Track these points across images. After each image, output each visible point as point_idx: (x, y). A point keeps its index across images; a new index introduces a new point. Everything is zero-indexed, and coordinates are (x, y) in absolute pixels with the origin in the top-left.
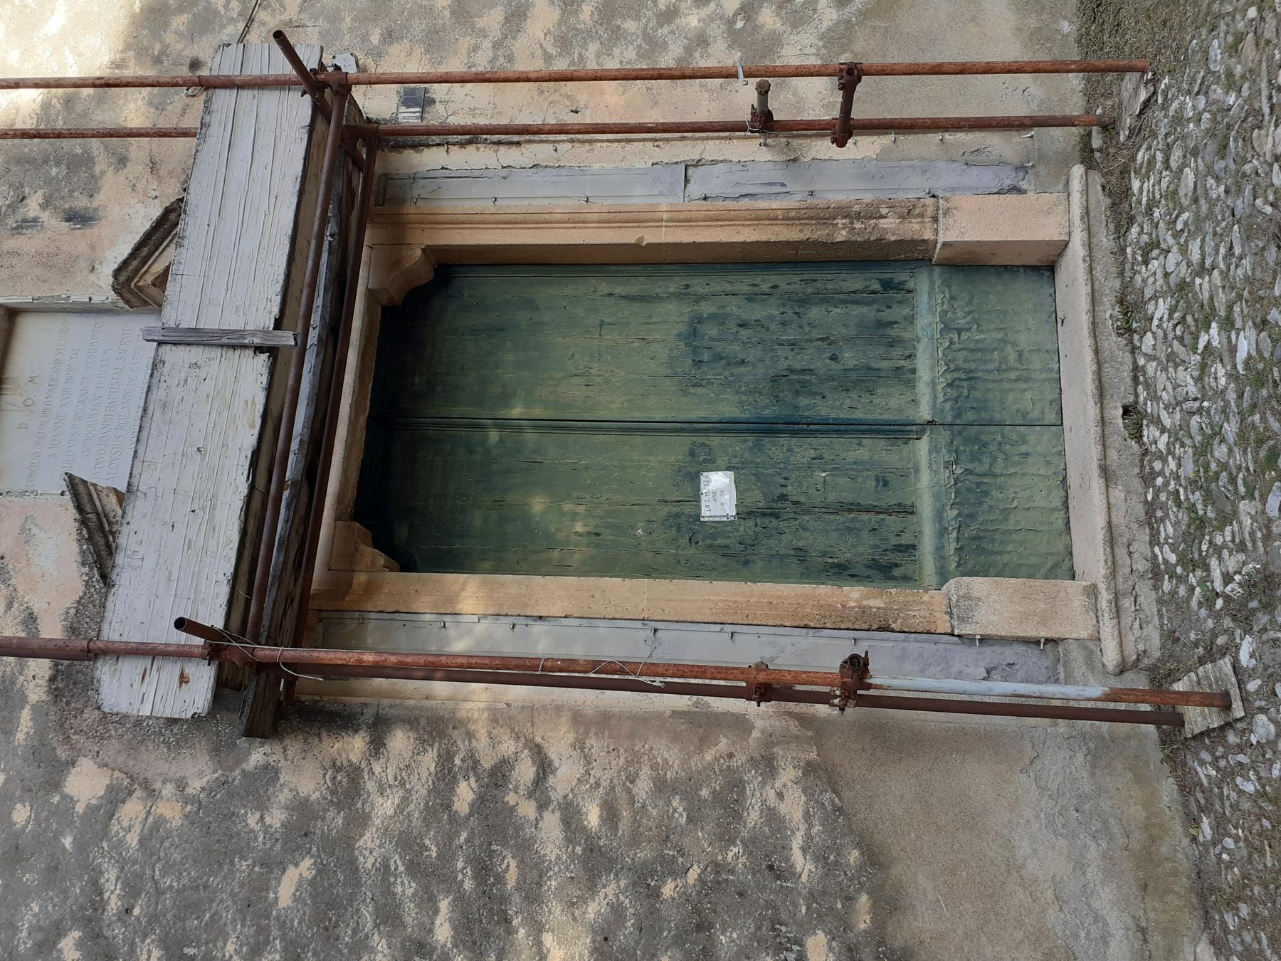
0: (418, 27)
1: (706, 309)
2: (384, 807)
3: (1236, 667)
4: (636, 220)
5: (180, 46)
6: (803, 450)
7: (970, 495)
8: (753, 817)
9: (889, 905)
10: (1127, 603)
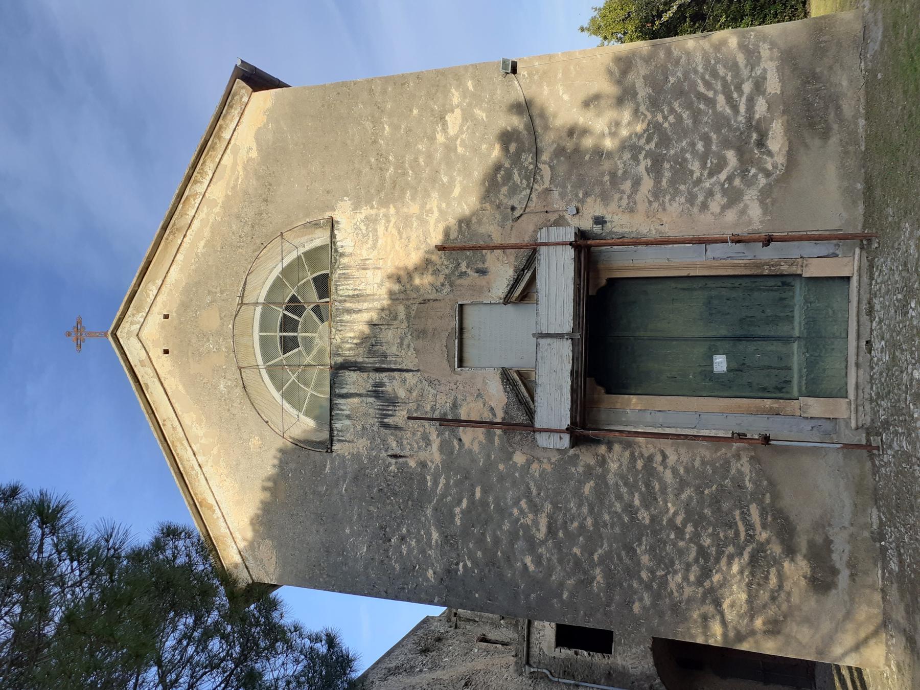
0: (597, 190)
1: (713, 293)
2: (613, 466)
3: (882, 440)
4: (688, 267)
5: (506, 201)
6: (751, 347)
7: (811, 364)
8: (733, 471)
9: (776, 496)
10: (860, 408)
